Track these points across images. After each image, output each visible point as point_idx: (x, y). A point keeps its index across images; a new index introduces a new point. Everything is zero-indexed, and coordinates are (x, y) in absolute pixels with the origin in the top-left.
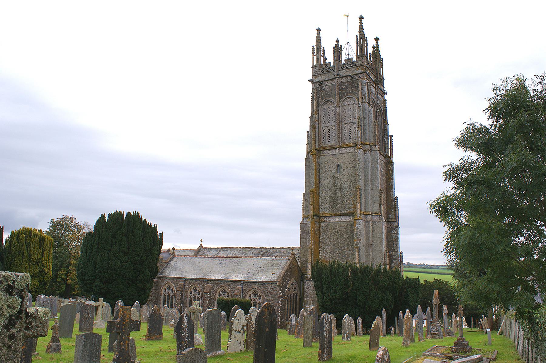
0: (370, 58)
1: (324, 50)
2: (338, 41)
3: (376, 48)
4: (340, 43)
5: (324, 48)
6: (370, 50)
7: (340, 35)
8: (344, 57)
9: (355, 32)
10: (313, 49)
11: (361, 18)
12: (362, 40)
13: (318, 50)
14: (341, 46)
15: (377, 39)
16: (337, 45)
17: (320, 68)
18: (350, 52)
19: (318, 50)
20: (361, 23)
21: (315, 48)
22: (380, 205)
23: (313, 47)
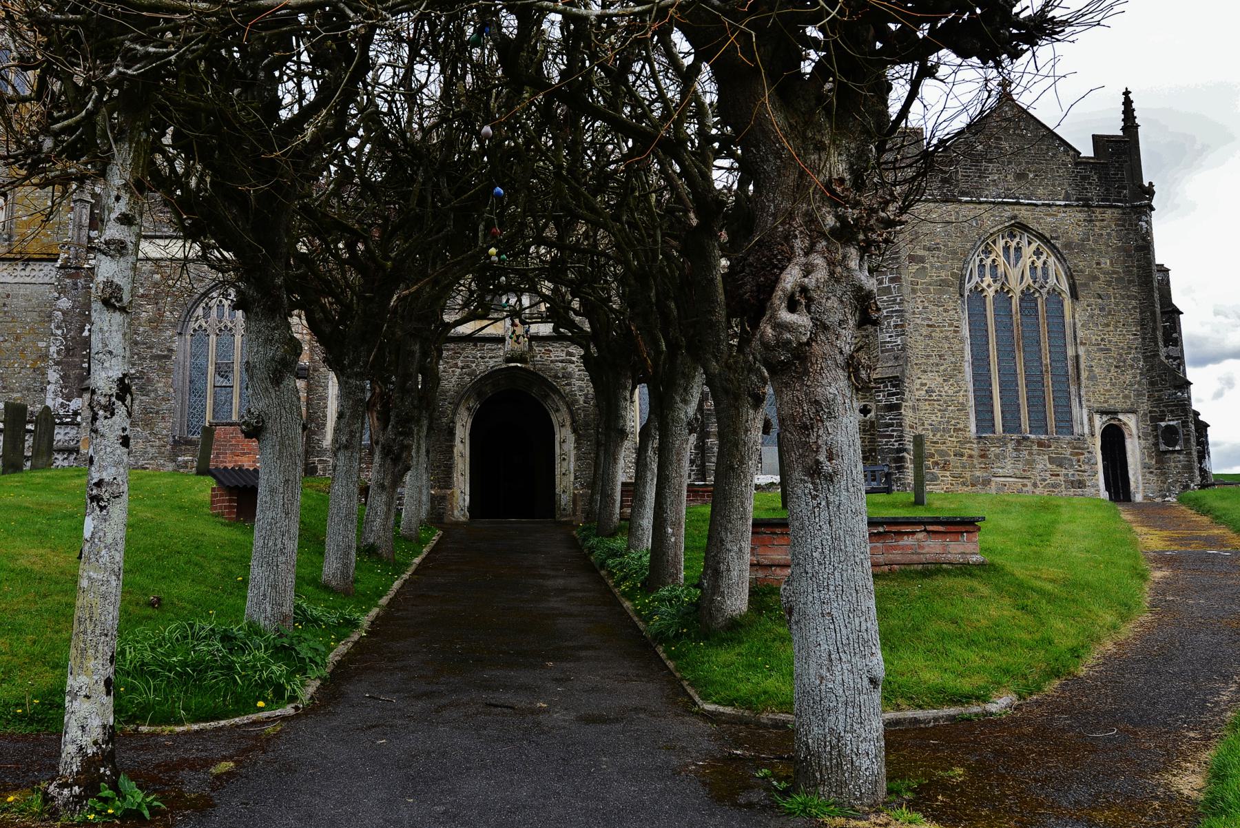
2: (1127, 93)
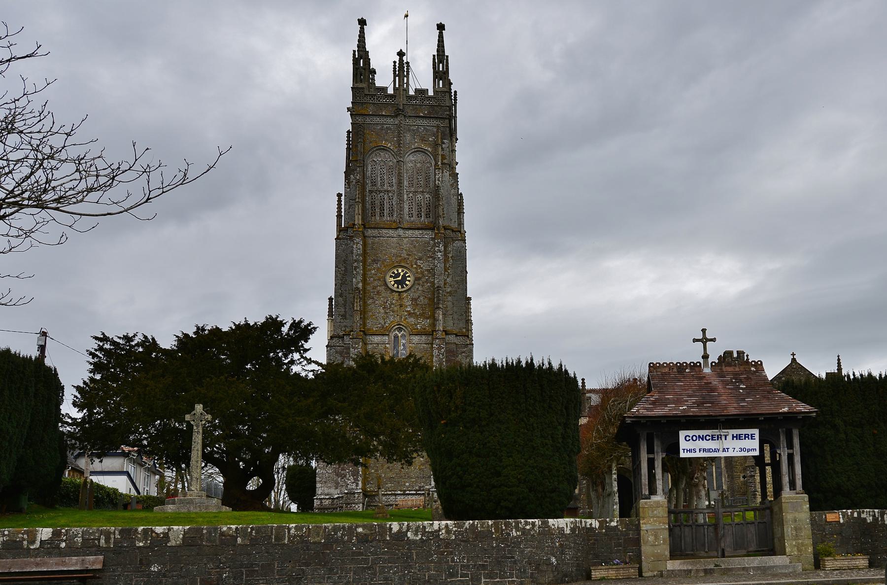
2: (401, 54)
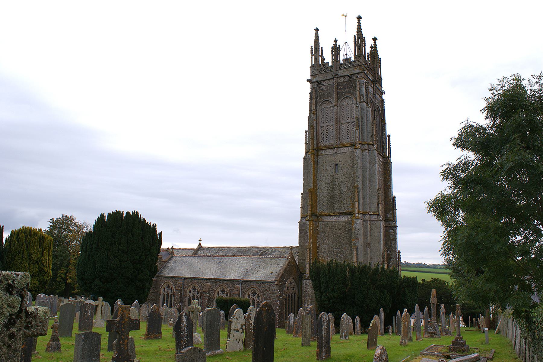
0: (368, 58)
1: (322, 50)
2: (336, 41)
3: (374, 48)
4: (338, 43)
5: (322, 48)
6: (368, 50)
7: (338, 35)
8: (342, 57)
9: (354, 32)
10: (312, 49)
11: (359, 18)
12: (360, 40)
13: (316, 50)
14: (339, 45)
15: (375, 39)
16: (335, 45)
17: (318, 68)
18: (348, 52)
19: (316, 50)
20: (359, 23)
21: (313, 48)
22: (378, 204)
23: (312, 47)
